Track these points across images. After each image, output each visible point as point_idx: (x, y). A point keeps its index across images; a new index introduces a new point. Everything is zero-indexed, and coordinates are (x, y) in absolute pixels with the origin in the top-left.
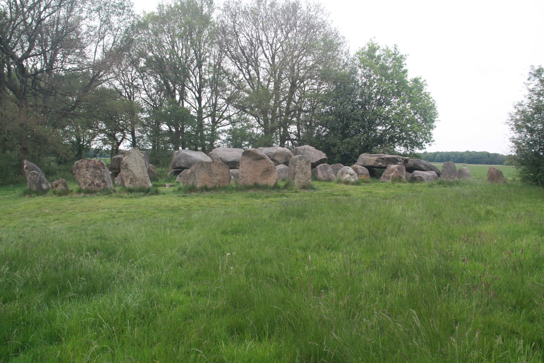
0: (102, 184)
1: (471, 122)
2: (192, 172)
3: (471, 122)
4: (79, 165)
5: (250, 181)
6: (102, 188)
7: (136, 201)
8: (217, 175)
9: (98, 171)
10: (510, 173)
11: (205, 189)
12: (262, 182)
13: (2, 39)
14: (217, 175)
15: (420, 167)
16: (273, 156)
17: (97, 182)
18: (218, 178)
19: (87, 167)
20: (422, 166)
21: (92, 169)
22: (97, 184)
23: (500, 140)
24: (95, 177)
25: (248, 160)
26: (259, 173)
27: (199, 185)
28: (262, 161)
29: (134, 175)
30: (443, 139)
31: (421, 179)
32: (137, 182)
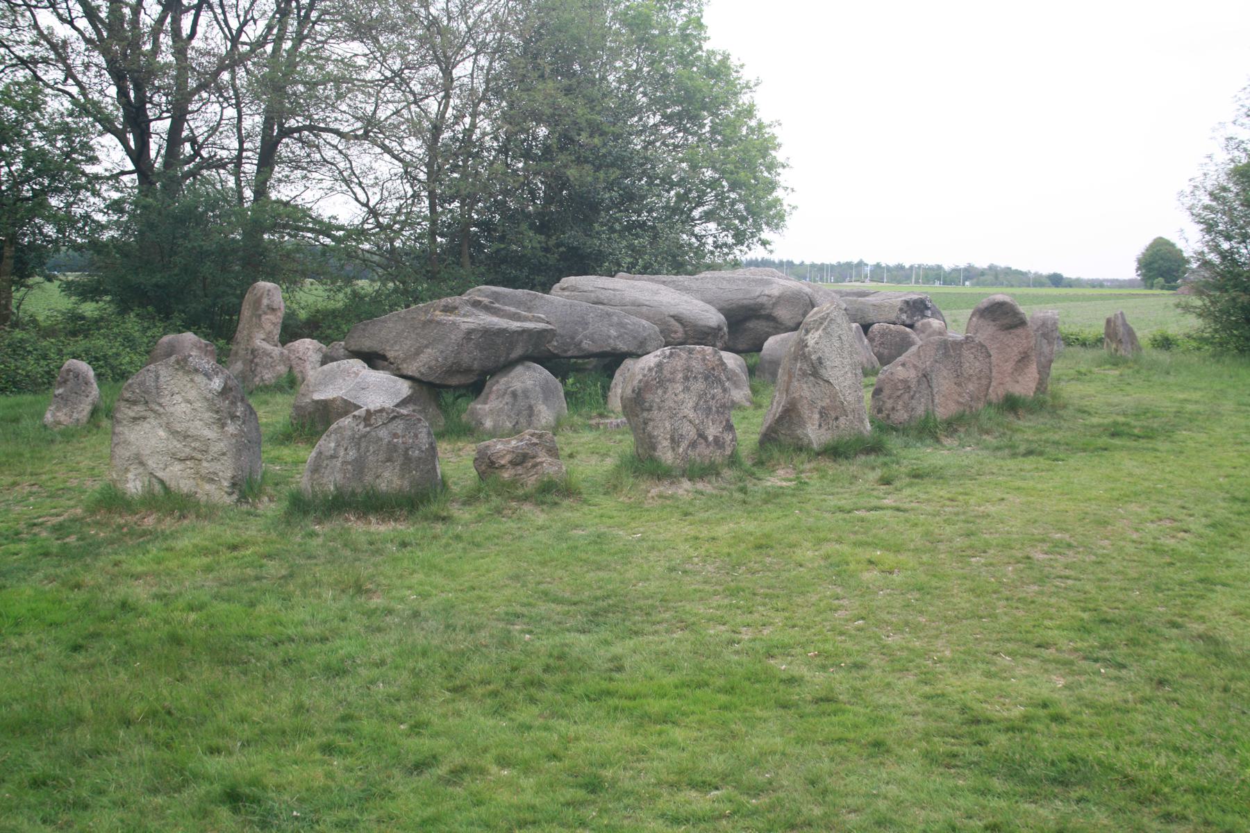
0: (728, 437)
6: (728, 452)
16: (774, 304)
21: (699, 385)
28: (1019, 331)
29: (834, 397)
32: (842, 420)
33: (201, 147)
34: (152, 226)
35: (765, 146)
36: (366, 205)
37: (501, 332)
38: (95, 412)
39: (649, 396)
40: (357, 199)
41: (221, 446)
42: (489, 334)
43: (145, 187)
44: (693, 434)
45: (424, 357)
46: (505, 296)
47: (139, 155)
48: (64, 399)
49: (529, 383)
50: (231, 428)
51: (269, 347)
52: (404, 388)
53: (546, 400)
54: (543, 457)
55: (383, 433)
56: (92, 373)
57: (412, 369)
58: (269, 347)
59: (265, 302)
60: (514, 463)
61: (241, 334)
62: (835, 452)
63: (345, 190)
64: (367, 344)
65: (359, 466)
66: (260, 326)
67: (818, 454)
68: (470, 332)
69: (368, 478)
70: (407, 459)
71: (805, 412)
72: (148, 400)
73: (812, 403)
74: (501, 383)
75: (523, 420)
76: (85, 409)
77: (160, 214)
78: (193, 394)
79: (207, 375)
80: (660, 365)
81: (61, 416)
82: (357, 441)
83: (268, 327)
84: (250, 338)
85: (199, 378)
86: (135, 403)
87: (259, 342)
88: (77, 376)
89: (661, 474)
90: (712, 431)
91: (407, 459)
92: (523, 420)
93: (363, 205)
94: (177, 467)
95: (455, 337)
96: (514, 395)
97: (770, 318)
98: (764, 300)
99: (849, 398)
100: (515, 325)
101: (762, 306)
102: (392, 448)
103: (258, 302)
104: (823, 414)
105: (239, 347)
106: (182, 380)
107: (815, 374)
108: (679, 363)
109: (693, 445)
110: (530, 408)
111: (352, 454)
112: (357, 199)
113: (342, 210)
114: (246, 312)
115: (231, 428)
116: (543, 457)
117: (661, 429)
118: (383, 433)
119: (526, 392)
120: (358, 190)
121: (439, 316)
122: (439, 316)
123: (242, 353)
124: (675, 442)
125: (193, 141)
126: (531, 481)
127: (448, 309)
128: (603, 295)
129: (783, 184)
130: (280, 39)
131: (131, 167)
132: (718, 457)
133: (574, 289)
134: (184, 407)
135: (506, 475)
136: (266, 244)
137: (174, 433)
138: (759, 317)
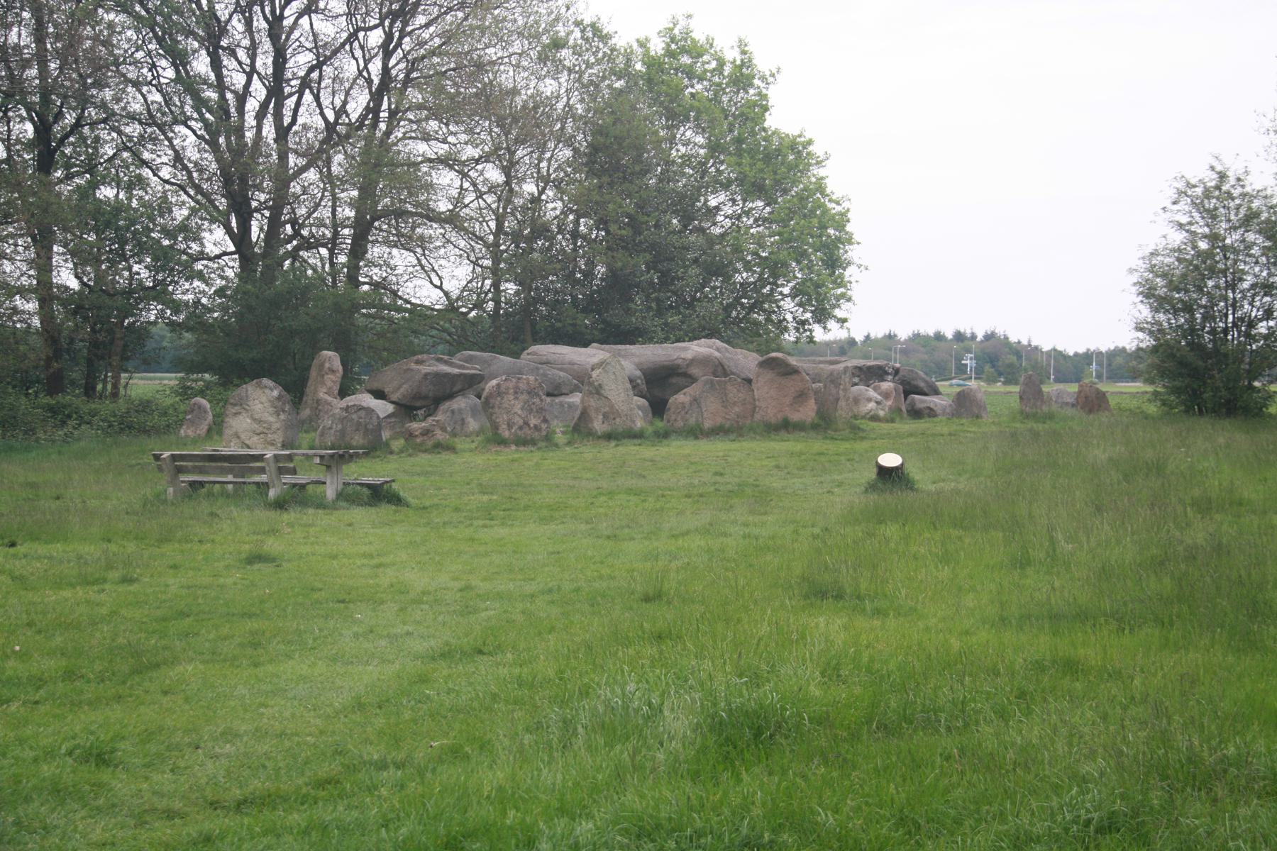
0: (544, 426)
1: (988, 220)
2: (695, 400)
3: (988, 220)
4: (503, 389)
5: (772, 415)
6: (544, 433)
7: (621, 449)
8: (735, 403)
9: (537, 400)
10: (1130, 392)
11: (719, 431)
12: (795, 417)
13: (1275, 264)
14: (735, 403)
15: (917, 387)
16: (688, 365)
17: (533, 421)
18: (737, 409)
19: (517, 391)
20: (922, 384)
21: (525, 397)
22: (535, 426)
23: (1095, 313)
24: (531, 411)
25: (769, 375)
26: (787, 401)
27: (707, 425)
28: (795, 377)
29: (612, 406)
30: (888, 297)
31: (931, 413)
32: (618, 420)
33: (302, 226)
34: (250, 309)
35: (841, 221)
36: (440, 288)
37: (447, 375)
38: (209, 430)
39: (492, 401)
40: (431, 282)
41: (277, 425)
42: (439, 376)
43: (245, 275)
44: (521, 422)
45: (402, 390)
46: (476, 357)
47: (241, 239)
48: (192, 422)
49: (463, 405)
50: (282, 417)
51: (329, 399)
52: (390, 408)
53: (473, 416)
54: (438, 432)
55: (354, 416)
56: (208, 406)
57: (395, 397)
58: (329, 399)
59: (327, 365)
60: (422, 434)
61: (310, 389)
62: (609, 437)
63: (434, 276)
64: (376, 385)
65: (343, 433)
66: (323, 383)
67: (599, 437)
68: (426, 375)
69: (347, 439)
70: (367, 430)
71: (593, 414)
72: (242, 403)
73: (597, 410)
74: (445, 406)
75: (458, 427)
76: (204, 427)
77: (257, 297)
78: (264, 399)
79: (272, 390)
80: (498, 385)
81: (190, 432)
82: (342, 420)
83: (329, 384)
84: (316, 391)
85: (267, 391)
86: (235, 405)
87: (322, 395)
88: (199, 407)
89: (503, 442)
90: (533, 421)
91: (367, 430)
92: (458, 427)
93: (436, 286)
94: (256, 438)
95: (418, 377)
96: (453, 412)
97: (686, 375)
98: (680, 361)
99: (622, 407)
100: (456, 371)
101: (678, 366)
102: (359, 424)
103: (322, 365)
104: (605, 416)
105: (308, 399)
106: (259, 392)
107: (598, 393)
108: (511, 384)
109: (521, 428)
110: (463, 420)
111: (340, 426)
112: (431, 282)
113: (423, 293)
114: (313, 373)
115: (282, 417)
116: (438, 432)
117: (502, 419)
118: (354, 416)
119: (460, 410)
120: (433, 275)
121: (413, 366)
122: (413, 366)
123: (310, 402)
124: (510, 426)
125: (294, 222)
126: (430, 443)
127: (418, 362)
128: (551, 358)
129: (856, 260)
130: (375, 125)
131: (232, 248)
132: (536, 435)
133: (534, 354)
134: (260, 406)
135: (418, 440)
136: (362, 331)
137: (254, 420)
138: (679, 375)
